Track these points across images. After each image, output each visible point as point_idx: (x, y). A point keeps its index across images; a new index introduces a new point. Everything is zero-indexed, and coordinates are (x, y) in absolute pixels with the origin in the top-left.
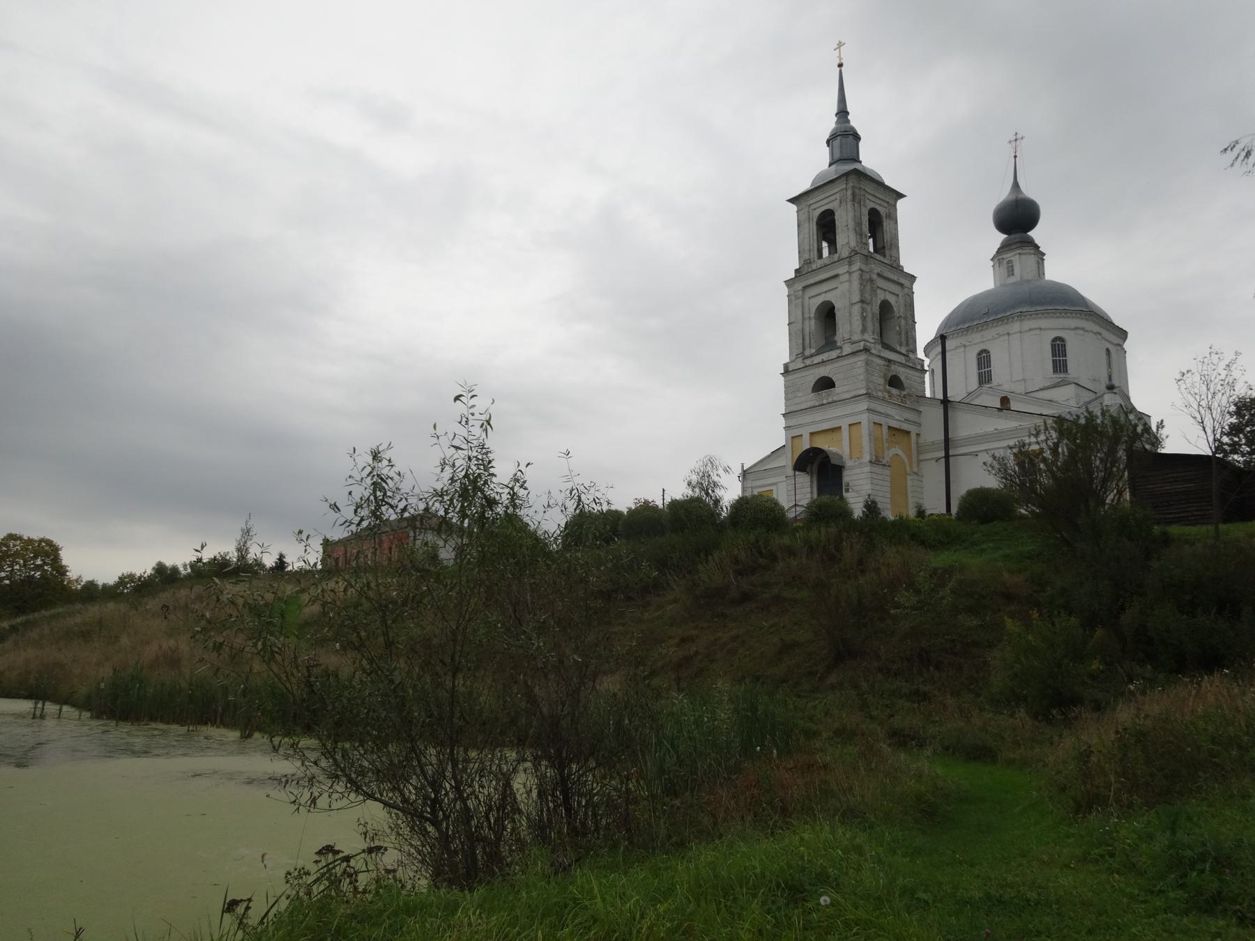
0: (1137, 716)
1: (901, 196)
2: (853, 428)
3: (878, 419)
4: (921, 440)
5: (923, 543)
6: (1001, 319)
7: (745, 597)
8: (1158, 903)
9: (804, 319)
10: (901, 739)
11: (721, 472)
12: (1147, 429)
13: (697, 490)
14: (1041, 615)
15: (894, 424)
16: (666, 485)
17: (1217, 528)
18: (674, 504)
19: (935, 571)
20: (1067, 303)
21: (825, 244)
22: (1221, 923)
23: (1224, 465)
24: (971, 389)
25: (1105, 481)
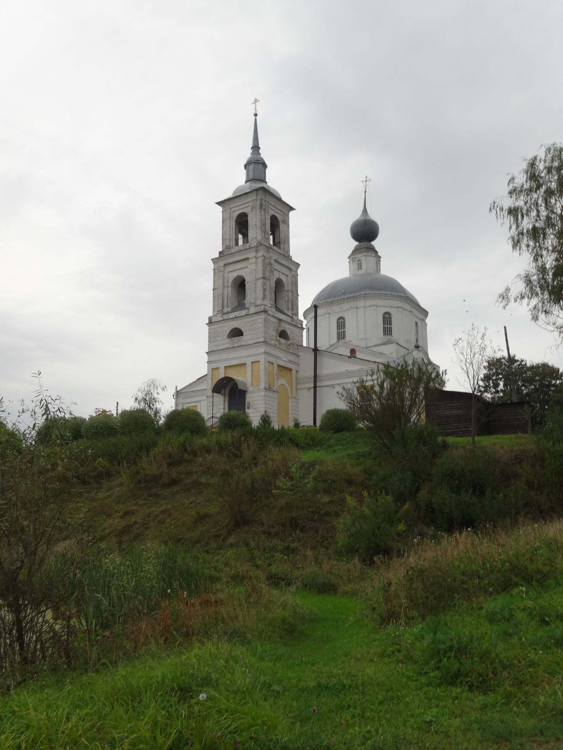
0: (419, 559)
1: (292, 209)
2: (254, 365)
3: (271, 359)
4: (299, 375)
5: (297, 445)
6: (353, 298)
7: (173, 482)
8: (423, 681)
9: (224, 287)
10: (275, 580)
11: (160, 390)
12: (438, 375)
13: (142, 404)
14: (369, 494)
15: (282, 363)
16: (119, 400)
17: (473, 440)
18: (125, 413)
19: (303, 464)
20: (393, 291)
21: (240, 236)
22: (459, 690)
23: (480, 399)
24: (332, 343)
25: (411, 407)
